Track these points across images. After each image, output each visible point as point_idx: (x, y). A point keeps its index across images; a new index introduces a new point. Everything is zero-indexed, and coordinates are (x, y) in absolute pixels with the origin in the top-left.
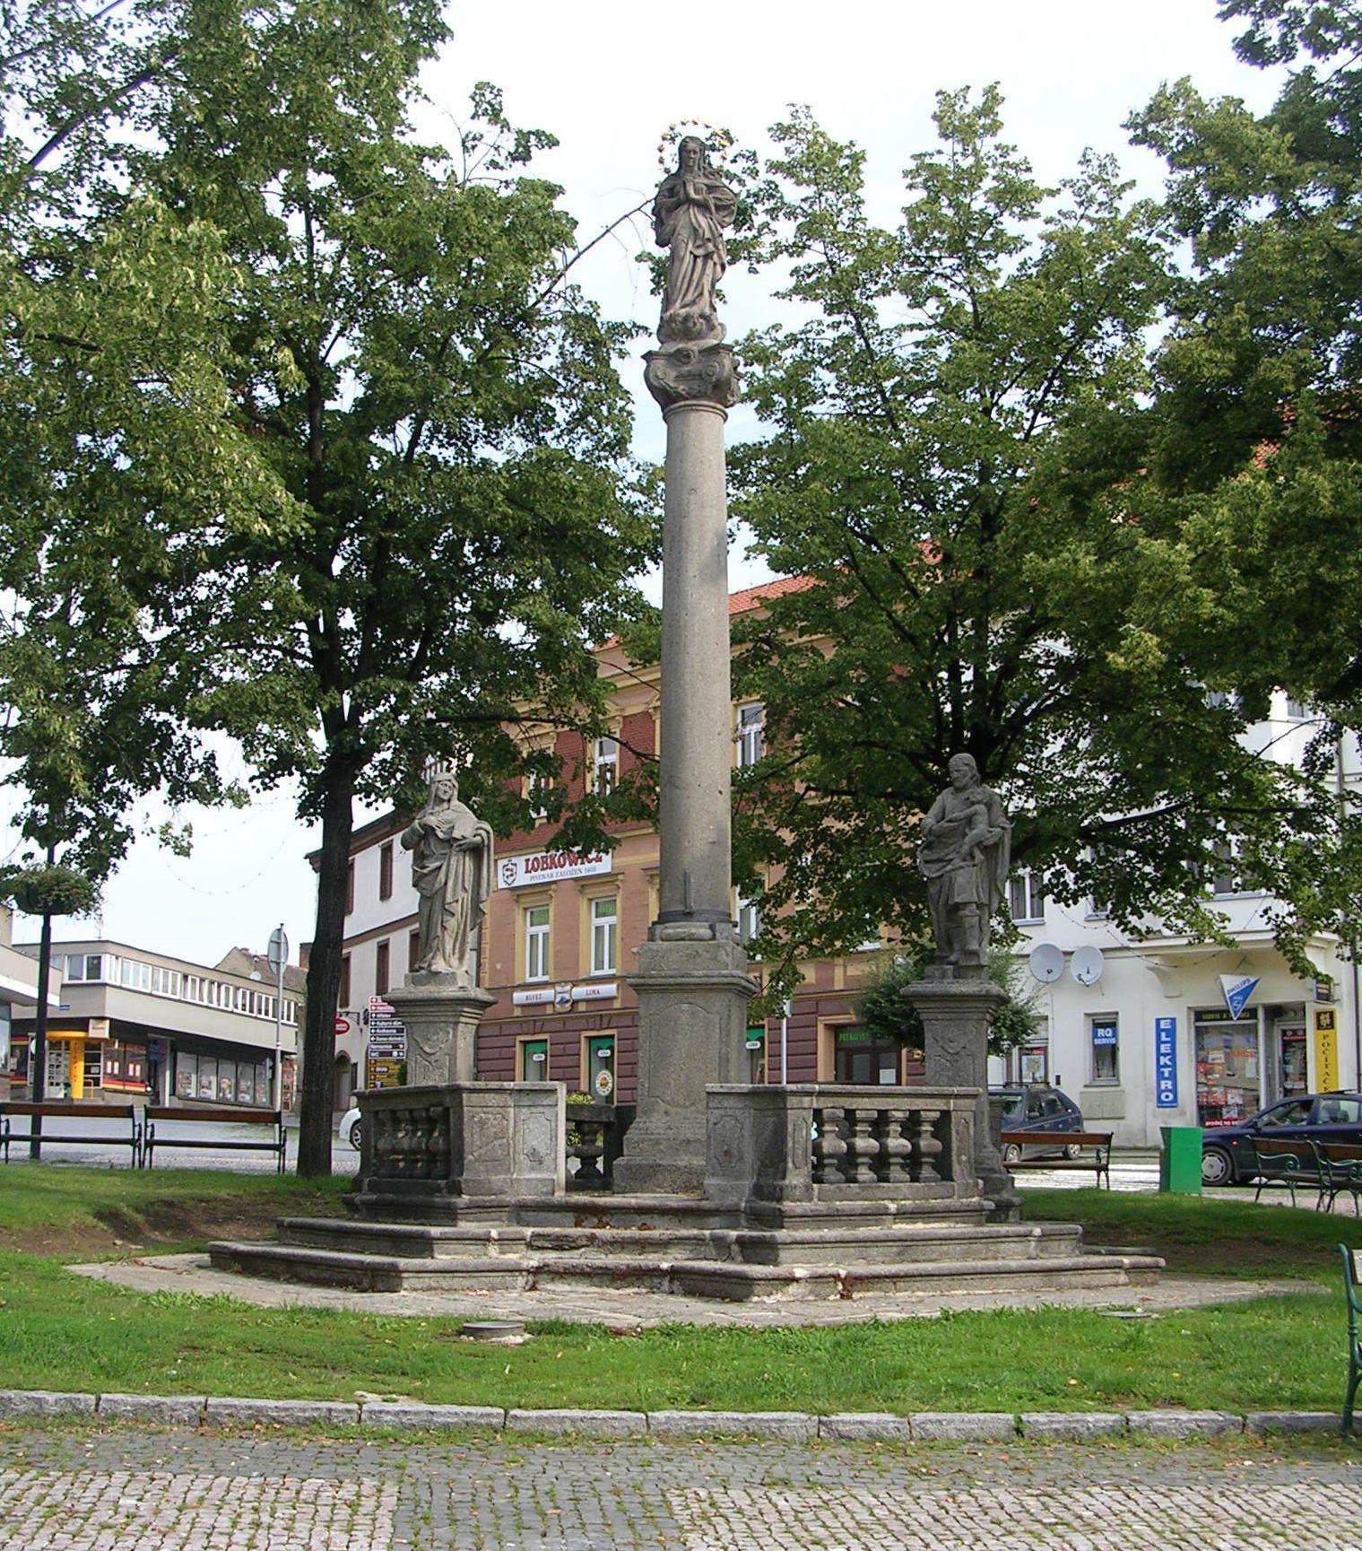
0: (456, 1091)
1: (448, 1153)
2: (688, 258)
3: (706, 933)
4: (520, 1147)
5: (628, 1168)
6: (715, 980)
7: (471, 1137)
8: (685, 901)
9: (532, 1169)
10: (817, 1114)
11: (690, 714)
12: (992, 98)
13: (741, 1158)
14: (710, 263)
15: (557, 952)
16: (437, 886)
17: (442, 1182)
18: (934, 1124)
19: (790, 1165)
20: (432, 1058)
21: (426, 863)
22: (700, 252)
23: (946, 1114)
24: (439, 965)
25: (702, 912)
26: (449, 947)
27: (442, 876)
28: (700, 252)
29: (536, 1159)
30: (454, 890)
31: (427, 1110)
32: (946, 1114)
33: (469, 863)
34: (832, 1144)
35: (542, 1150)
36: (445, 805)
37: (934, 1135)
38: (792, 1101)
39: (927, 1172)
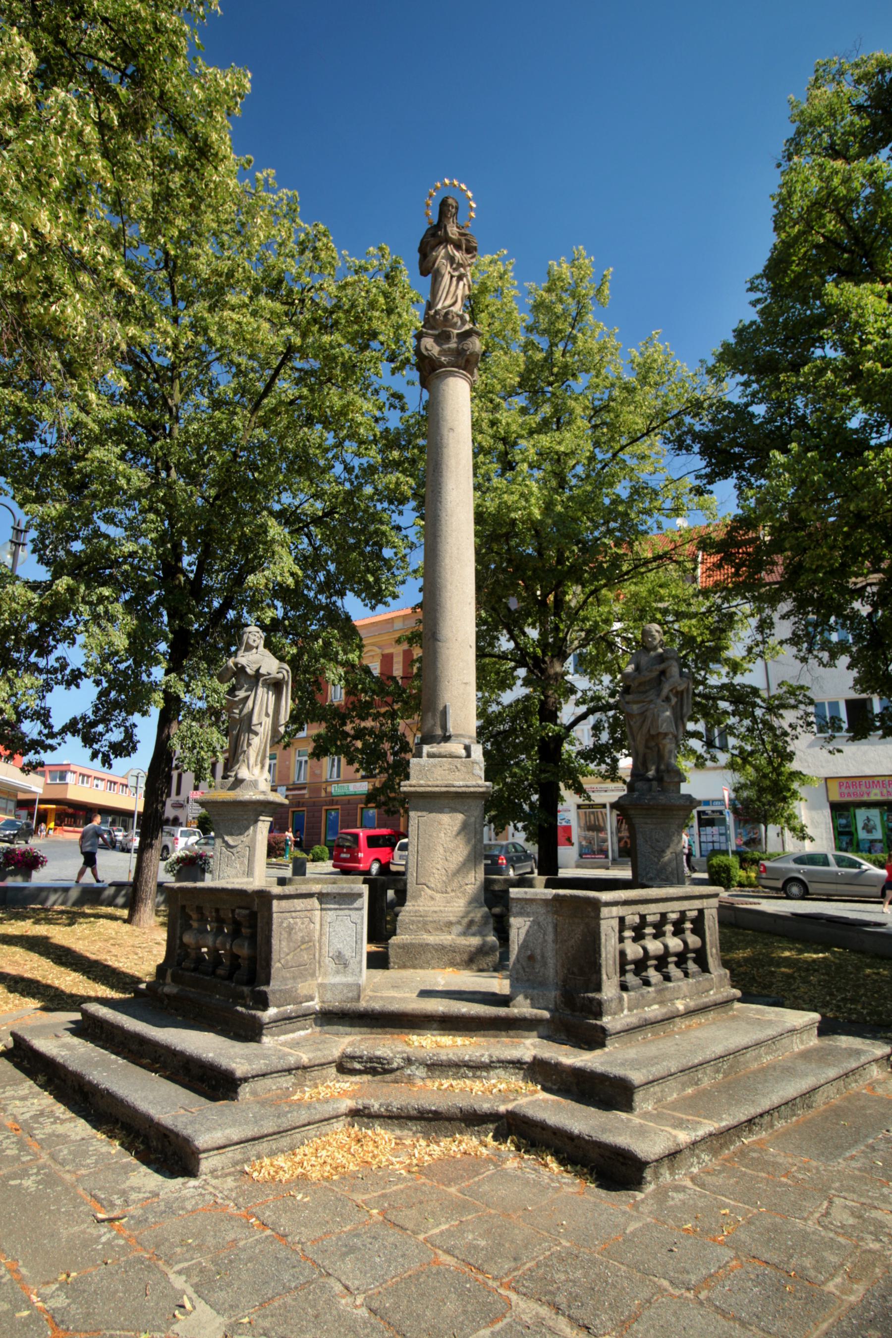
0: (264, 898)
1: (253, 960)
2: (447, 278)
3: (463, 753)
4: (325, 949)
5: (404, 947)
6: (472, 789)
7: (280, 945)
8: (444, 727)
9: (338, 972)
10: (622, 920)
11: (449, 587)
12: (13, 1034)
13: (545, 964)
14: (461, 284)
15: (280, 772)
16: (245, 711)
17: (246, 990)
18: (693, 921)
19: (604, 977)
20: (234, 850)
21: (237, 693)
22: (456, 274)
23: (701, 912)
24: (243, 773)
25: (457, 736)
26: (252, 761)
27: (250, 703)
28: (456, 274)
29: (341, 960)
30: (259, 715)
31: (233, 911)
32: (701, 912)
33: (272, 698)
34: (633, 951)
35: (348, 953)
36: (254, 651)
37: (694, 931)
38: (605, 912)
39: (692, 966)
